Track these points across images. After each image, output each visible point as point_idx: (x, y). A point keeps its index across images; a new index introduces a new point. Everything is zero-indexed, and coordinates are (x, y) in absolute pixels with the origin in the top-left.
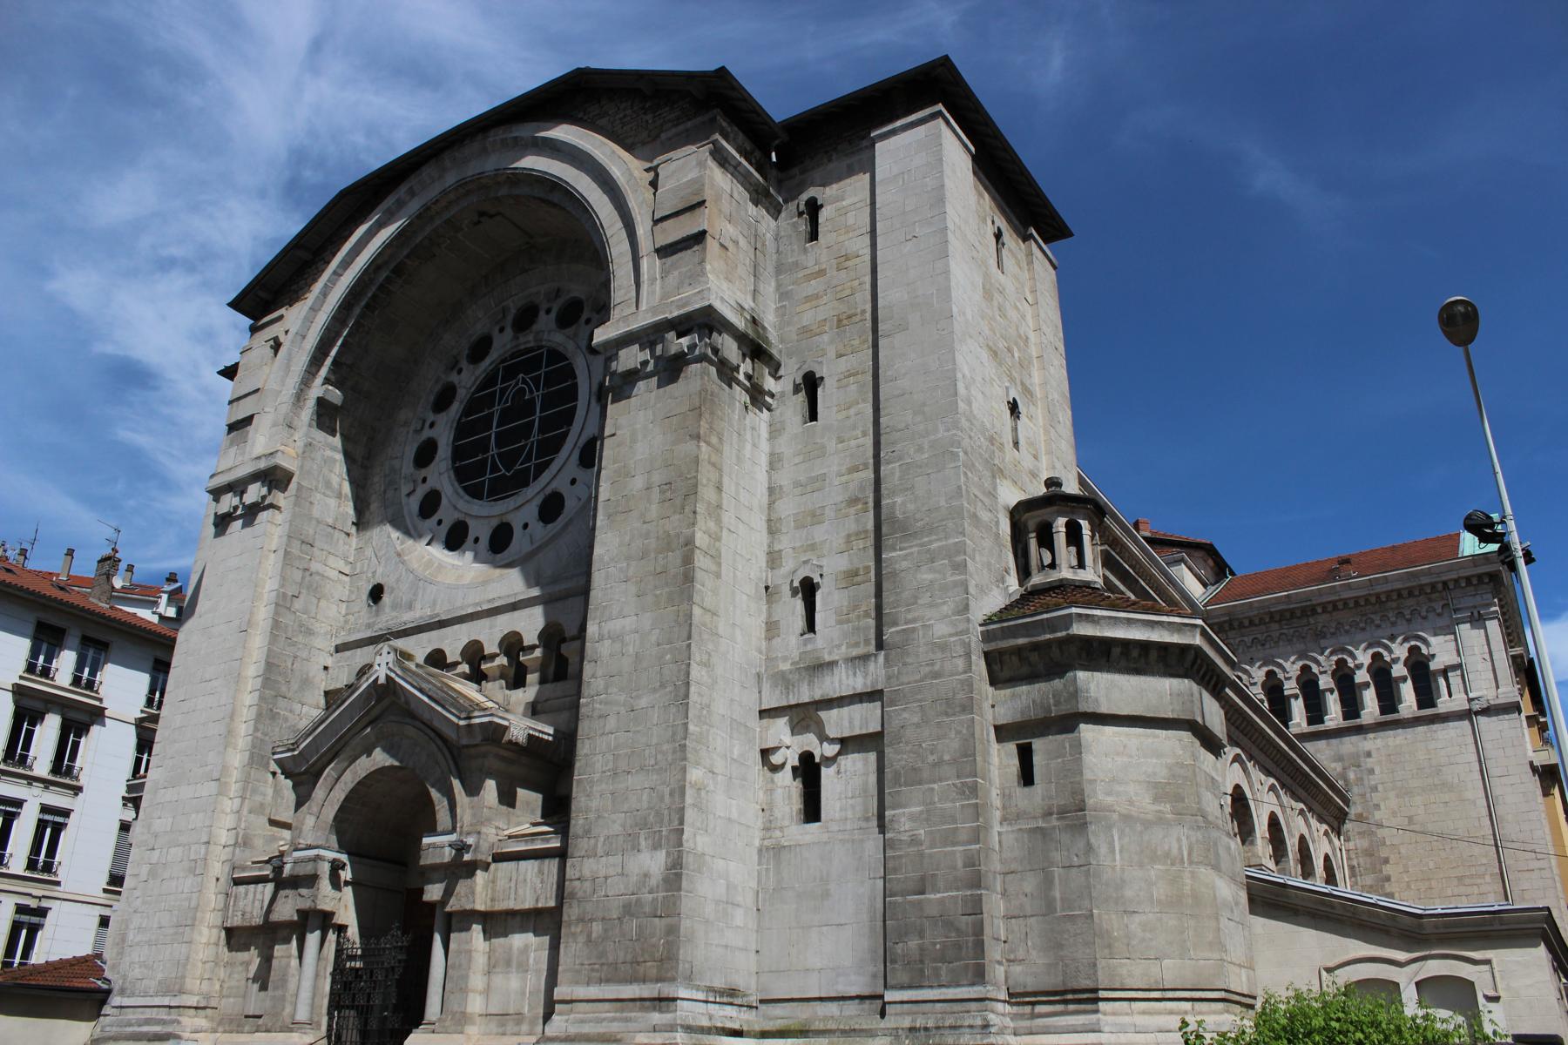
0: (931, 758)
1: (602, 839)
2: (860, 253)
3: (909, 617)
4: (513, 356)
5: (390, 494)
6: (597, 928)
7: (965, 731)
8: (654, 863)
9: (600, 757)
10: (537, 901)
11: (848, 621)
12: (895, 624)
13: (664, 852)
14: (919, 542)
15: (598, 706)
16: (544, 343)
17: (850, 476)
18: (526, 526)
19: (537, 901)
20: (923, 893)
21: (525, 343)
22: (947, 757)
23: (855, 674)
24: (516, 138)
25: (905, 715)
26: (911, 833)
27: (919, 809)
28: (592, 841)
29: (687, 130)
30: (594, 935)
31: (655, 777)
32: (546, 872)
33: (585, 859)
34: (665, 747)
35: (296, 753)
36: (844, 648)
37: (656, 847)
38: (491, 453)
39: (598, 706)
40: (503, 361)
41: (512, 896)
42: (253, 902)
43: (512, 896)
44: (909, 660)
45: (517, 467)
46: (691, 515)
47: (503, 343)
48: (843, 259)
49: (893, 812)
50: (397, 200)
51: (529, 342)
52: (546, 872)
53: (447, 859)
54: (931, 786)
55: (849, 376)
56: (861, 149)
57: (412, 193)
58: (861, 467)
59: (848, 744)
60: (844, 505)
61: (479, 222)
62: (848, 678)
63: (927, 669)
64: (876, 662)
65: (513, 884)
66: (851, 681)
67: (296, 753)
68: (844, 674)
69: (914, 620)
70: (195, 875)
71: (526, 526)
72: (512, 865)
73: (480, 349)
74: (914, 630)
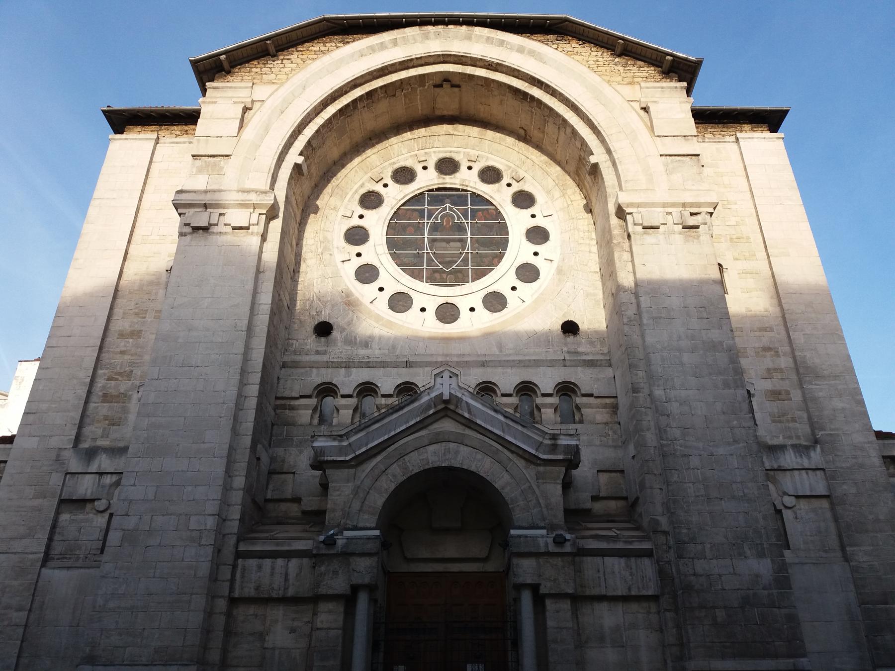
0: (870, 517)
1: (709, 546)
2: (738, 202)
3: (833, 427)
4: (438, 189)
5: (326, 256)
6: (720, 614)
7: (890, 503)
8: (763, 567)
9: (691, 485)
10: (629, 589)
11: (780, 422)
12: (822, 429)
13: (769, 560)
14: (828, 382)
15: (679, 447)
16: (469, 189)
17: (761, 333)
18: (381, 289)
19: (629, 589)
20: (887, 603)
21: (451, 184)
22: (881, 517)
23: (801, 456)
24: (503, 41)
25: (845, 487)
26: (869, 563)
27: (869, 548)
28: (699, 547)
29: (662, 88)
30: (719, 620)
31: (746, 505)
32: (634, 567)
33: (696, 560)
34: (750, 485)
35: (345, 443)
36: (781, 438)
37: (761, 555)
38: (466, 251)
39: (679, 447)
40: (429, 191)
41: (603, 584)
42: (272, 574)
43: (603, 584)
44: (838, 453)
45: (441, 267)
46: (729, 332)
47: (427, 179)
48: (726, 203)
49: (852, 549)
50: (382, 43)
51: (455, 184)
52: (634, 567)
53: (241, 560)
54: (875, 534)
55: (747, 273)
56: (725, 142)
57: (395, 43)
58: (768, 329)
59: (346, 364)
60: (760, 350)
61: (441, 86)
62: (796, 458)
63: (854, 461)
64: (815, 450)
65: (601, 575)
66: (799, 460)
67: (345, 443)
68: (792, 455)
69: (837, 429)
70: (200, 545)
71: (381, 289)
72: (599, 559)
73: (491, 175)
74: (838, 435)
